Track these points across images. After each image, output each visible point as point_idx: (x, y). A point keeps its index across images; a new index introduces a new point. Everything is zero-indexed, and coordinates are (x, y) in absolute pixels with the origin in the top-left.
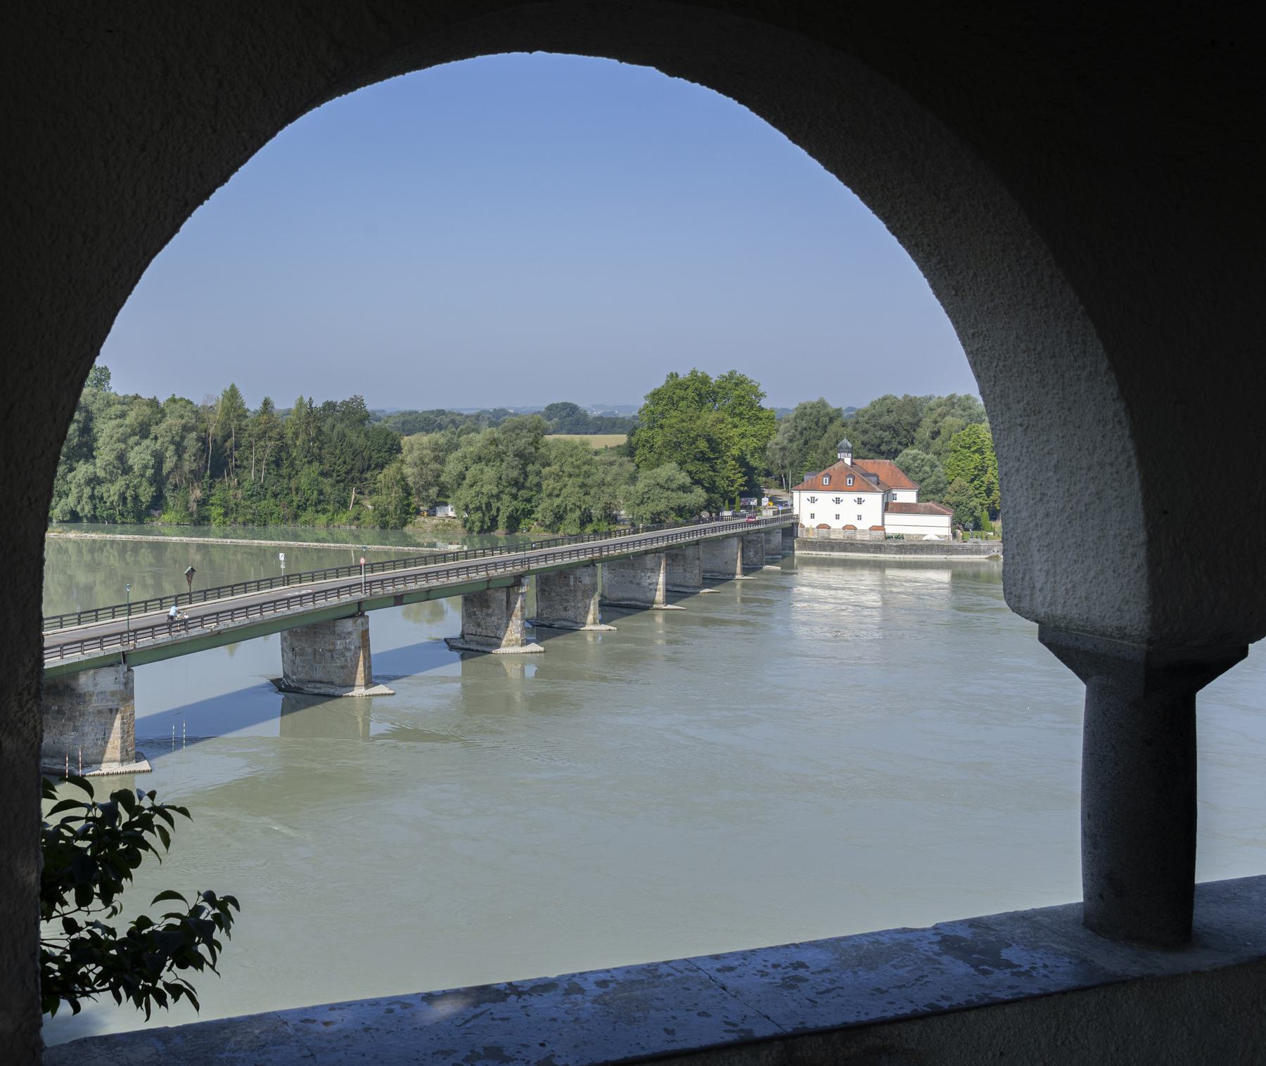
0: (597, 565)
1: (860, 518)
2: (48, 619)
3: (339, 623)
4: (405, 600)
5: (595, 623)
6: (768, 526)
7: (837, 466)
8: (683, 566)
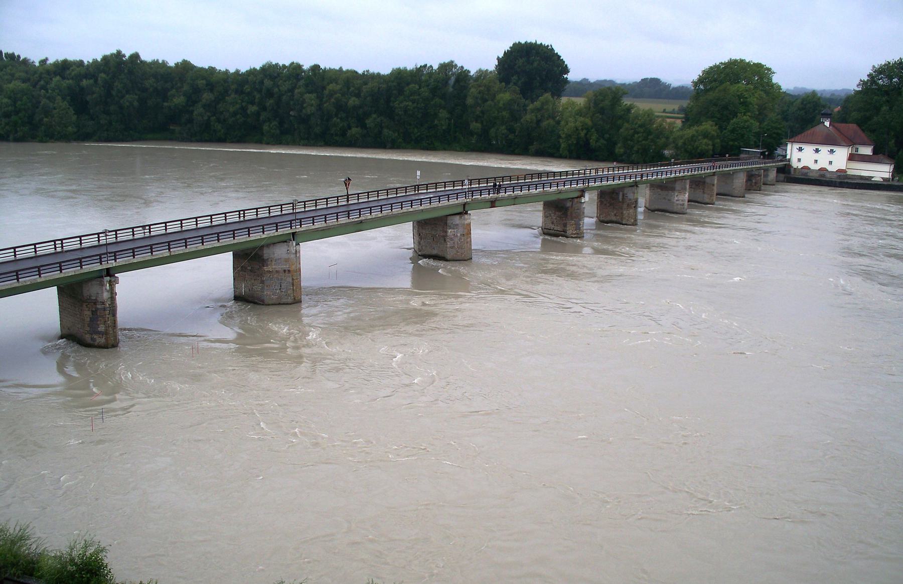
1: (831, 163)
3: (449, 218)
4: (497, 203)
5: (766, 170)
6: (766, 165)
7: (820, 126)
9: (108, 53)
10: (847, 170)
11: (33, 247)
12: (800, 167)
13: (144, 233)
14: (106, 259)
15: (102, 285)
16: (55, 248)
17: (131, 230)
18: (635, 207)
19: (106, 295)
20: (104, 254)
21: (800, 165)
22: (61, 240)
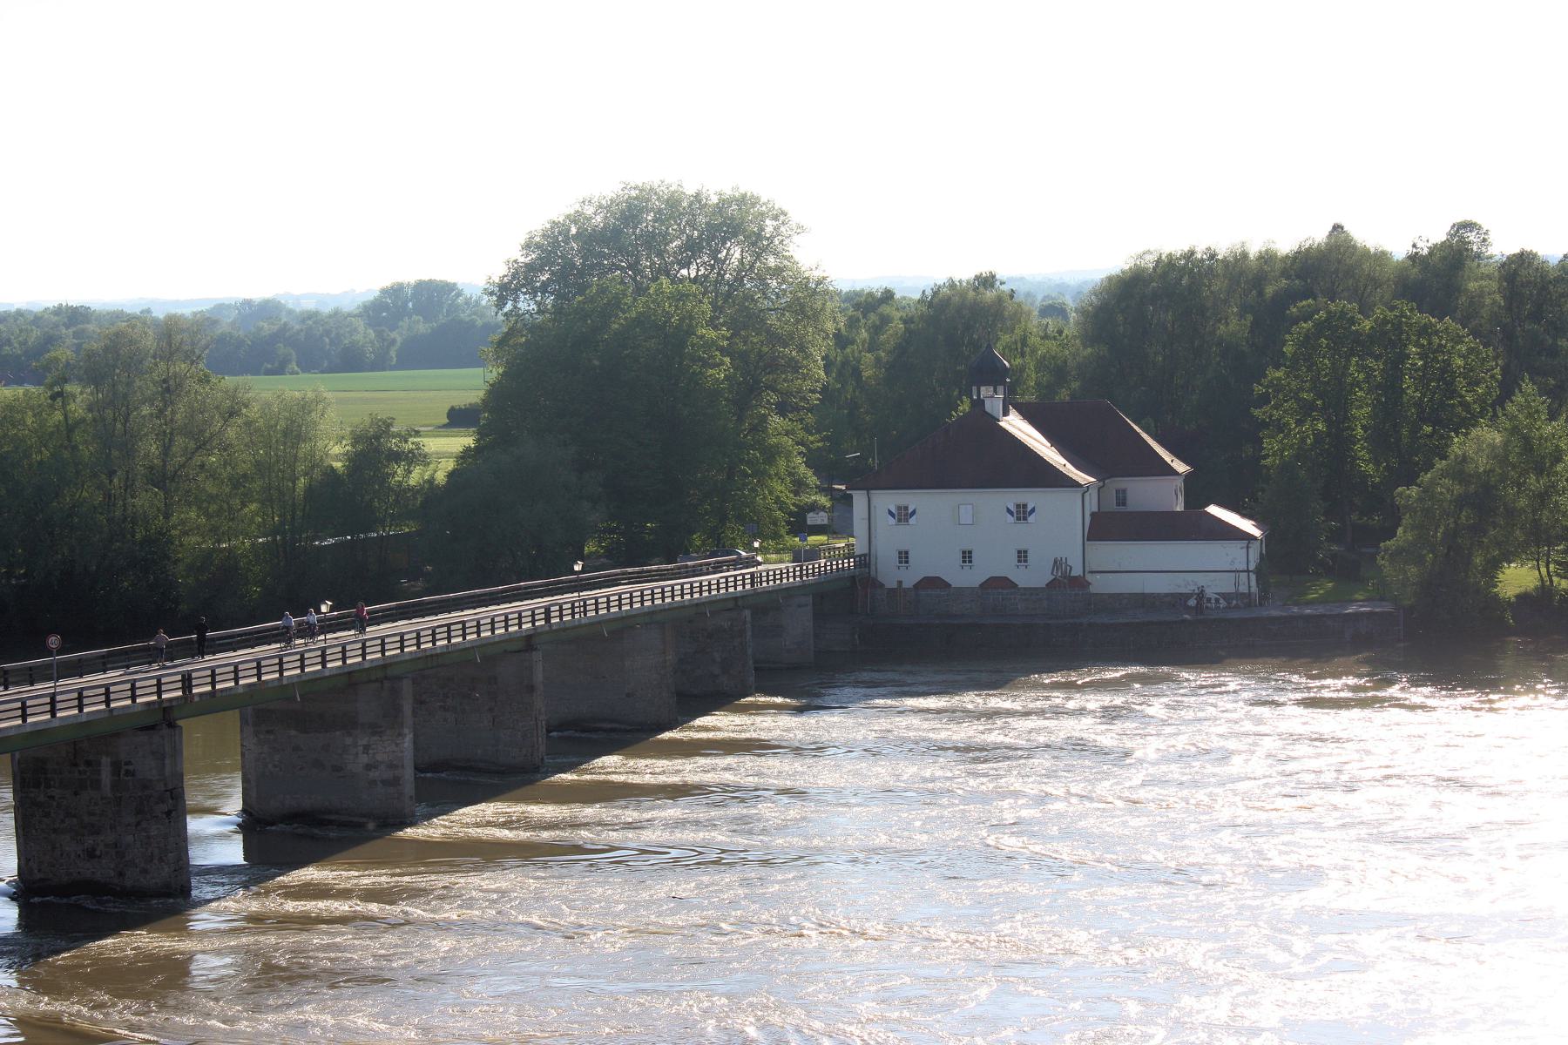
0: (180, 723)
2: (195, 678)
8: (491, 710)
9: (423, 278)
10: (1089, 577)
12: (909, 583)
18: (168, 813)
21: (910, 578)
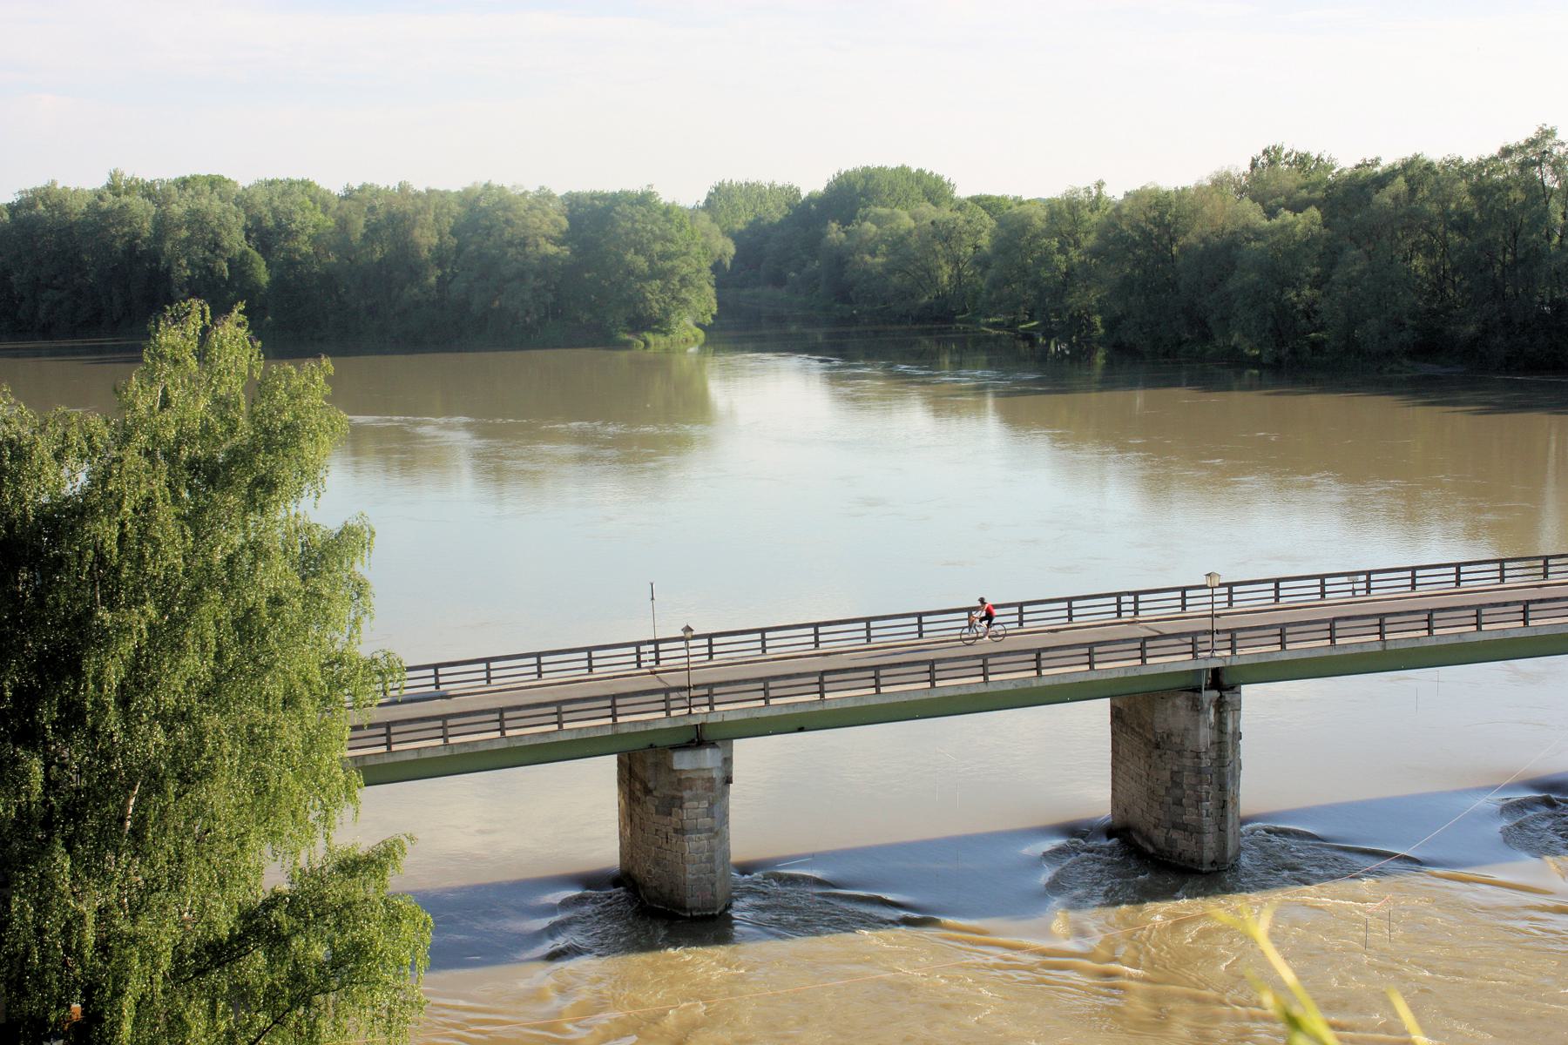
11: (534, 660)
13: (1353, 591)
14: (1208, 646)
15: (1196, 707)
16: (1119, 612)
17: (915, 620)
19: (1205, 735)
20: (1205, 632)
22: (1136, 594)
